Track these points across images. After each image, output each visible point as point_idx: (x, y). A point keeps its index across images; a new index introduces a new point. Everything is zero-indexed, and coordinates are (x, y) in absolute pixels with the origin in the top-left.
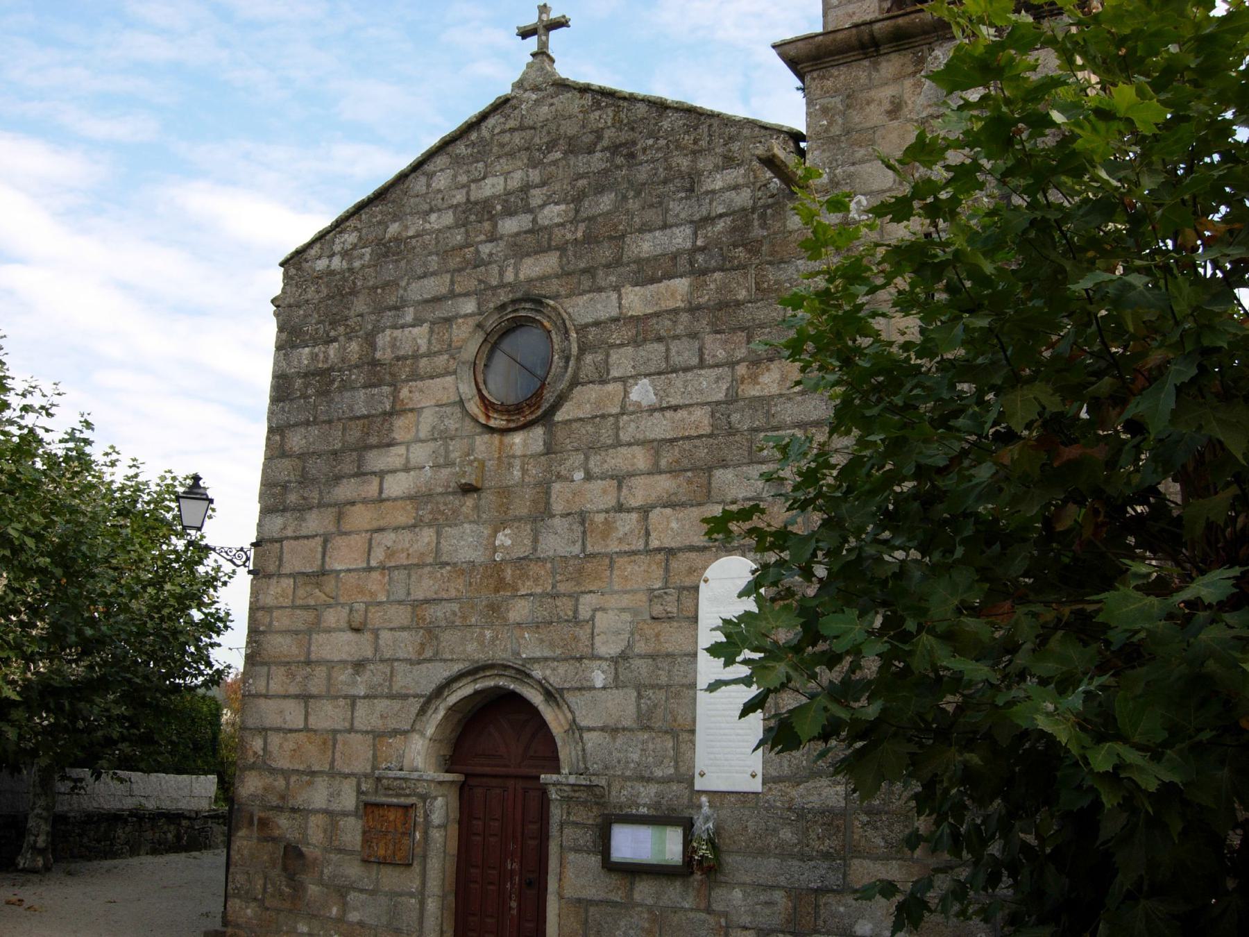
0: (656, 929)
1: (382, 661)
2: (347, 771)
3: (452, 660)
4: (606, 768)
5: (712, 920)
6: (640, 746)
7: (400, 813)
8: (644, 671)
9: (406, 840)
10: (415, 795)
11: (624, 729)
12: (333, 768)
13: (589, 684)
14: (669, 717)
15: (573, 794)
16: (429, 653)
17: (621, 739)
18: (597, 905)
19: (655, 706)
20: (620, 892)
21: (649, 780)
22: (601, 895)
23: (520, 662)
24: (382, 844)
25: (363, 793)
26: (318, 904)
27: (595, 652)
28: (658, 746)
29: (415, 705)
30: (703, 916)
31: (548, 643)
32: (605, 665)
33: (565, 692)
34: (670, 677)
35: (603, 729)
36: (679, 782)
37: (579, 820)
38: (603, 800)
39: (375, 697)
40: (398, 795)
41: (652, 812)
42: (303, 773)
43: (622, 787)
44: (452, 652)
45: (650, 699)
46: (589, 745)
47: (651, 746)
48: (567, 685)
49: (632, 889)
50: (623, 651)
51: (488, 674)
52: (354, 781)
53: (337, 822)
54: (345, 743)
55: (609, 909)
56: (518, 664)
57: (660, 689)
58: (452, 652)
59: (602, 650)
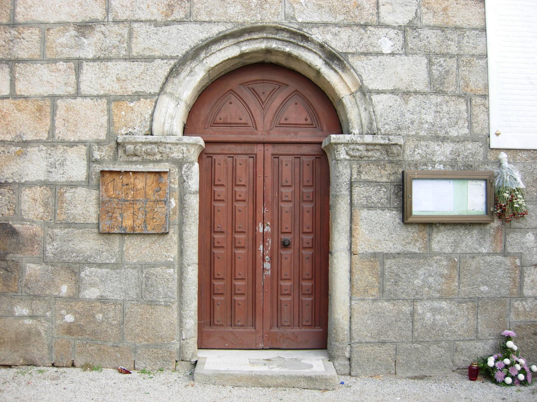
0: (455, 273)
1: (116, 22)
2: (72, 139)
3: (210, 22)
4: (399, 128)
5: (508, 261)
6: (434, 108)
7: (151, 179)
8: (433, 40)
9: (160, 209)
10: (167, 161)
11: (416, 92)
12: (53, 136)
13: (376, 49)
14: (462, 83)
15: (365, 153)
16: (179, 14)
17: (413, 101)
18: (394, 257)
19: (447, 72)
20: (417, 244)
21: (444, 139)
22: (399, 248)
23: (296, 26)
24: (128, 214)
25: (96, 161)
26: (41, 284)
27: (382, 21)
28: (452, 109)
29: (165, 69)
30: (500, 258)
31: (327, 9)
32: (392, 33)
33: (349, 56)
34: (460, 48)
35: (393, 92)
36: (473, 141)
37: (371, 178)
38: (398, 158)
39: (109, 59)
40: (144, 162)
41: (449, 168)
42: (11, 143)
43: (416, 146)
44: (210, 13)
45: (441, 66)
46: (379, 108)
47: (445, 108)
48: (350, 50)
49: (430, 240)
50: (410, 22)
51: (255, 36)
52: (83, 149)
53: (62, 194)
54: (68, 110)
55: (407, 260)
56: (294, 27)
57: (450, 58)
58: (210, 13)
59: (387, 18)
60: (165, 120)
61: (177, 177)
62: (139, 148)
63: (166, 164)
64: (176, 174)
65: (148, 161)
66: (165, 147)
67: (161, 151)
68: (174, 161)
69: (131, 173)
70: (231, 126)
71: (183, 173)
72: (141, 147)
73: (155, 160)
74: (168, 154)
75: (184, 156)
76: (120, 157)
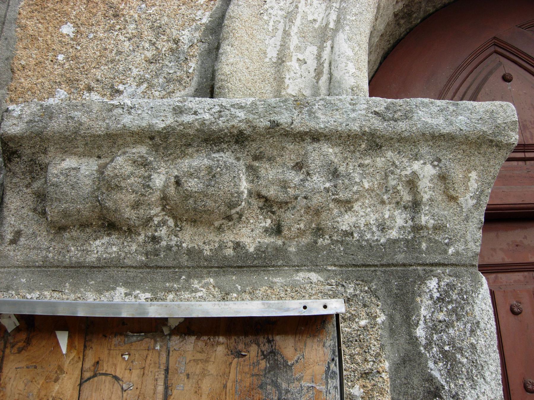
60: (284, 46)
61: (386, 365)
62: (129, 169)
63: (301, 276)
64: (375, 348)
65: (184, 260)
66: (299, 166)
67: (272, 192)
68: (360, 258)
69: (63, 339)
70: (524, 160)
71: (420, 332)
72: (145, 164)
73: (229, 252)
74: (317, 212)
75: (424, 219)
76: (14, 242)
